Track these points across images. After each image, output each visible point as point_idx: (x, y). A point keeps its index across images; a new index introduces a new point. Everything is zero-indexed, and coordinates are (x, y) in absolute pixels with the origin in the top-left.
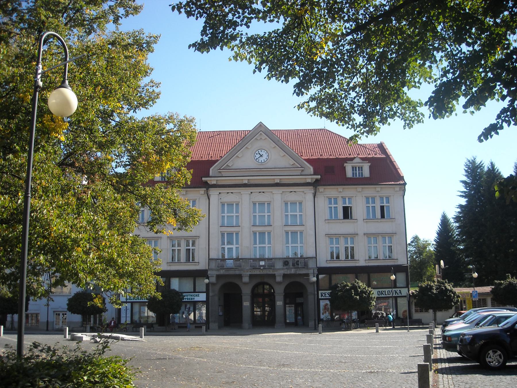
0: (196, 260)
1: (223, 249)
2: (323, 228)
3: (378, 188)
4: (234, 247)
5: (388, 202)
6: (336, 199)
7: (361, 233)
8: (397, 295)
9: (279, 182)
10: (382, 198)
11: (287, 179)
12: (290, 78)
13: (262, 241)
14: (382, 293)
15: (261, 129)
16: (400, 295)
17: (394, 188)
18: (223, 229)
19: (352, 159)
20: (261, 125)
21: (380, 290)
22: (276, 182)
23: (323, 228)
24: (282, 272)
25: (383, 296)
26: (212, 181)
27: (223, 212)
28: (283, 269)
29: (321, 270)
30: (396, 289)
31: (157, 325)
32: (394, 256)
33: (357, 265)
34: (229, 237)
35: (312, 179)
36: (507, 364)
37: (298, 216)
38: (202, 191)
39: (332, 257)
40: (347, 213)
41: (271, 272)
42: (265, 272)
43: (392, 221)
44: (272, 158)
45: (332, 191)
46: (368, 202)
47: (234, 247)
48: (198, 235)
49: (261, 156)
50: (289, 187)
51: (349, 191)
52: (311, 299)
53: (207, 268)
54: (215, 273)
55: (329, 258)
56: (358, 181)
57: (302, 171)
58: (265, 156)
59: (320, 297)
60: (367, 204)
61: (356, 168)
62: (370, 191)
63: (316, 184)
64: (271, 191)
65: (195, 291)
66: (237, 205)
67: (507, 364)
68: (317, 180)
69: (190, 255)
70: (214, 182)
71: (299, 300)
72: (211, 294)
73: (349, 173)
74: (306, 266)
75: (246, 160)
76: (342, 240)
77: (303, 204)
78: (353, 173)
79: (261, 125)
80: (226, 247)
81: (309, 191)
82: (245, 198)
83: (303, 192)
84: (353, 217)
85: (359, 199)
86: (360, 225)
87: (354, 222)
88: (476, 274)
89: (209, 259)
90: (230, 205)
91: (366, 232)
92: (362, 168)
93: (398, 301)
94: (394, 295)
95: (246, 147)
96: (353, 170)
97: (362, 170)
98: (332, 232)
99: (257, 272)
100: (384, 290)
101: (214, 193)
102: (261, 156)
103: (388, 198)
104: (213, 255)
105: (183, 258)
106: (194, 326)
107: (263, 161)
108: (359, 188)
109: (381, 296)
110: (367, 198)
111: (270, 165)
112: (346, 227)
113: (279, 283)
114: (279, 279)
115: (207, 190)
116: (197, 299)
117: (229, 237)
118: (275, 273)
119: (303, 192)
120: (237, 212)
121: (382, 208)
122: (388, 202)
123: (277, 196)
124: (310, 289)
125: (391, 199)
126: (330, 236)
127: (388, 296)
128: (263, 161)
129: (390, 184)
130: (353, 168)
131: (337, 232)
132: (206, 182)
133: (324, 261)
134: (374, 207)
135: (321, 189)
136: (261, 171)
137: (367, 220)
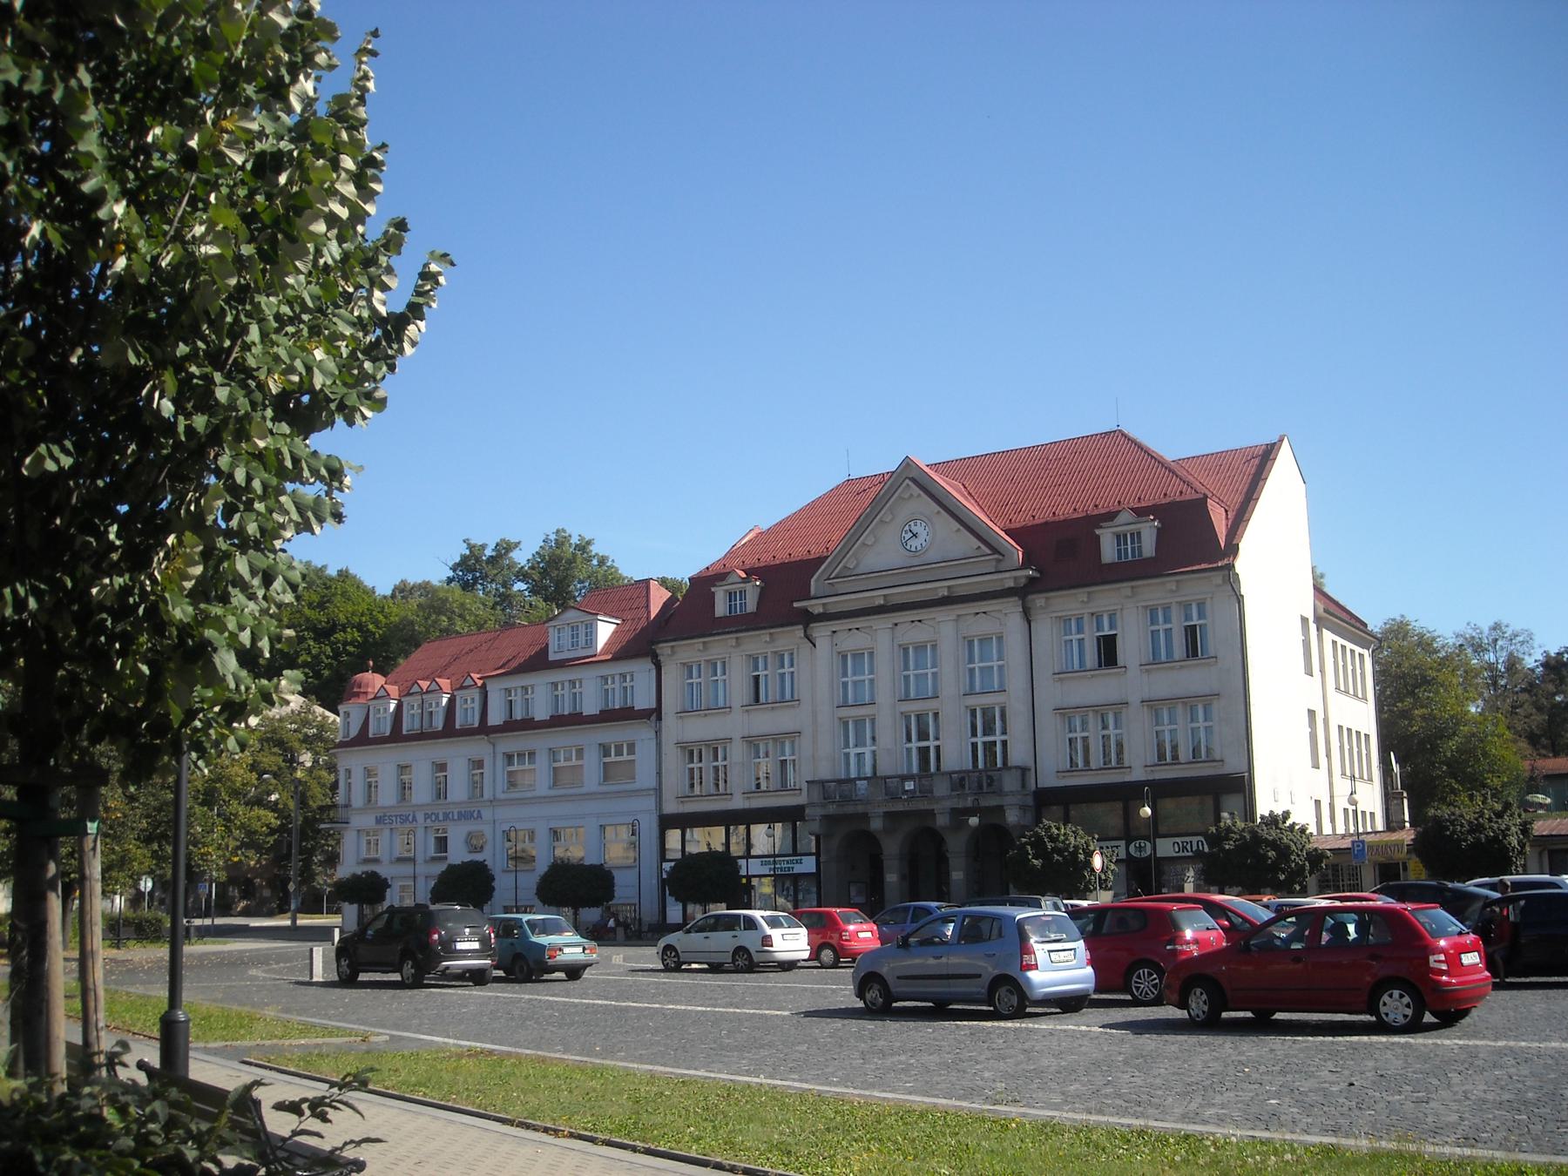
2: (1050, 694)
3: (1170, 583)
5: (1201, 615)
6: (1079, 620)
7: (1134, 699)
10: (1186, 606)
11: (963, 586)
12: (489, 552)
14: (1185, 848)
15: (909, 477)
18: (844, 712)
19: (1111, 516)
20: (907, 463)
21: (1178, 840)
23: (1050, 694)
24: (948, 804)
26: (816, 607)
28: (949, 797)
33: (1127, 779)
34: (856, 728)
36: (1224, 1015)
38: (798, 631)
39: (1161, 756)
40: (1108, 652)
41: (923, 805)
42: (913, 806)
44: (932, 537)
45: (1070, 603)
46: (1153, 621)
47: (867, 750)
49: (915, 535)
51: (1106, 598)
54: (819, 811)
56: (1132, 571)
57: (999, 561)
58: (923, 534)
62: (1156, 591)
63: (1022, 592)
65: (795, 853)
67: (1224, 1015)
68: (1031, 580)
70: (818, 610)
73: (1109, 553)
75: (883, 552)
76: (1093, 722)
79: (907, 463)
80: (853, 751)
82: (880, 636)
84: (1120, 662)
85: (1130, 614)
86: (1132, 682)
88: (150, 884)
90: (858, 656)
92: (1139, 533)
95: (881, 521)
99: (899, 807)
100: (1188, 839)
101: (821, 631)
102: (915, 535)
103: (1201, 606)
108: (1125, 587)
110: (1153, 612)
111: (932, 556)
112: (1103, 688)
116: (798, 869)
121: (1191, 632)
122: (1201, 615)
123: (944, 628)
126: (1063, 712)
129: (1193, 572)
132: (805, 611)
134: (1168, 632)
135: (1038, 600)
137: (1154, 662)
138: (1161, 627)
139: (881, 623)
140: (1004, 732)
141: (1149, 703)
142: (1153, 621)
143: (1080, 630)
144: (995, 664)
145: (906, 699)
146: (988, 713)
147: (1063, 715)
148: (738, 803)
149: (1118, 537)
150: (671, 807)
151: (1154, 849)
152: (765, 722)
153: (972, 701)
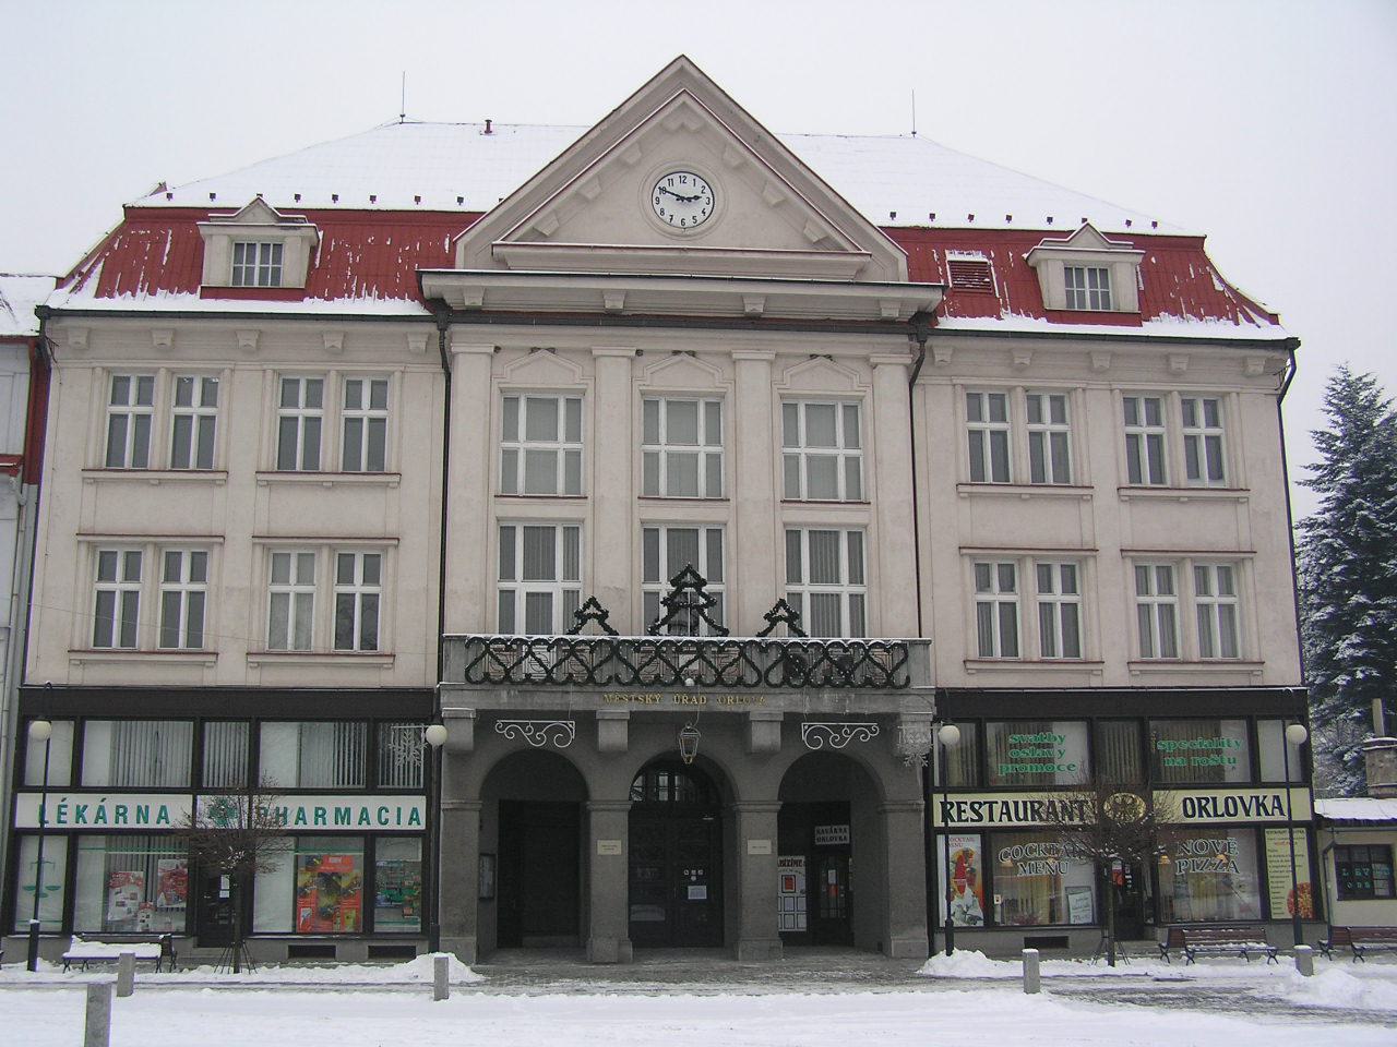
0: (383, 643)
1: (507, 597)
4: (556, 588)
7: (1108, 547)
8: (1264, 818)
9: (760, 309)
10: (1034, 403)
13: (825, 570)
16: (1277, 817)
17: (1167, 357)
18: (796, 515)
21: (1194, 794)
22: (748, 309)
25: (1205, 819)
27: (510, 433)
29: (951, 705)
30: (1260, 793)
31: (191, 942)
32: (1249, 646)
33: (1095, 682)
35: (902, 302)
37: (561, 457)
43: (1237, 501)
48: (392, 529)
50: (214, 320)
52: (902, 834)
53: (430, 680)
55: (974, 653)
59: (938, 822)
60: (971, 418)
61: (1080, 271)
64: (727, 348)
66: (574, 404)
69: (357, 626)
71: (831, 835)
72: (446, 801)
74: (891, 684)
76: (1186, 579)
77: (866, 411)
78: (1069, 294)
81: (891, 361)
83: (866, 359)
87: (386, 485)
89: (441, 640)
91: (87, 525)
93: (1269, 845)
94: (1253, 817)
96: (1069, 283)
97: (1105, 284)
98: (282, 525)
101: (472, 350)
104: (461, 623)
105: (323, 631)
106: (366, 945)
107: (689, 222)
109: (1196, 819)
113: (764, 756)
114: (613, 736)
115: (442, 330)
117: (538, 548)
118: (748, 708)
119: (866, 359)
120: (574, 434)
123: (753, 380)
124: (900, 788)
125: (393, 394)
127: (1227, 819)
128: (689, 222)
130: (1068, 270)
131: (1006, 540)
133: (951, 662)
136: (681, 264)
138: (131, 409)
139: (614, 348)
140: (857, 576)
141: (263, 540)
142: (119, 397)
143: (144, 398)
144: (841, 452)
145: (507, 493)
146: (824, 539)
147: (92, 546)
148: (231, 671)
149: (239, 246)
150: (50, 668)
151: (1150, 807)
152: (310, 510)
153: (796, 515)
